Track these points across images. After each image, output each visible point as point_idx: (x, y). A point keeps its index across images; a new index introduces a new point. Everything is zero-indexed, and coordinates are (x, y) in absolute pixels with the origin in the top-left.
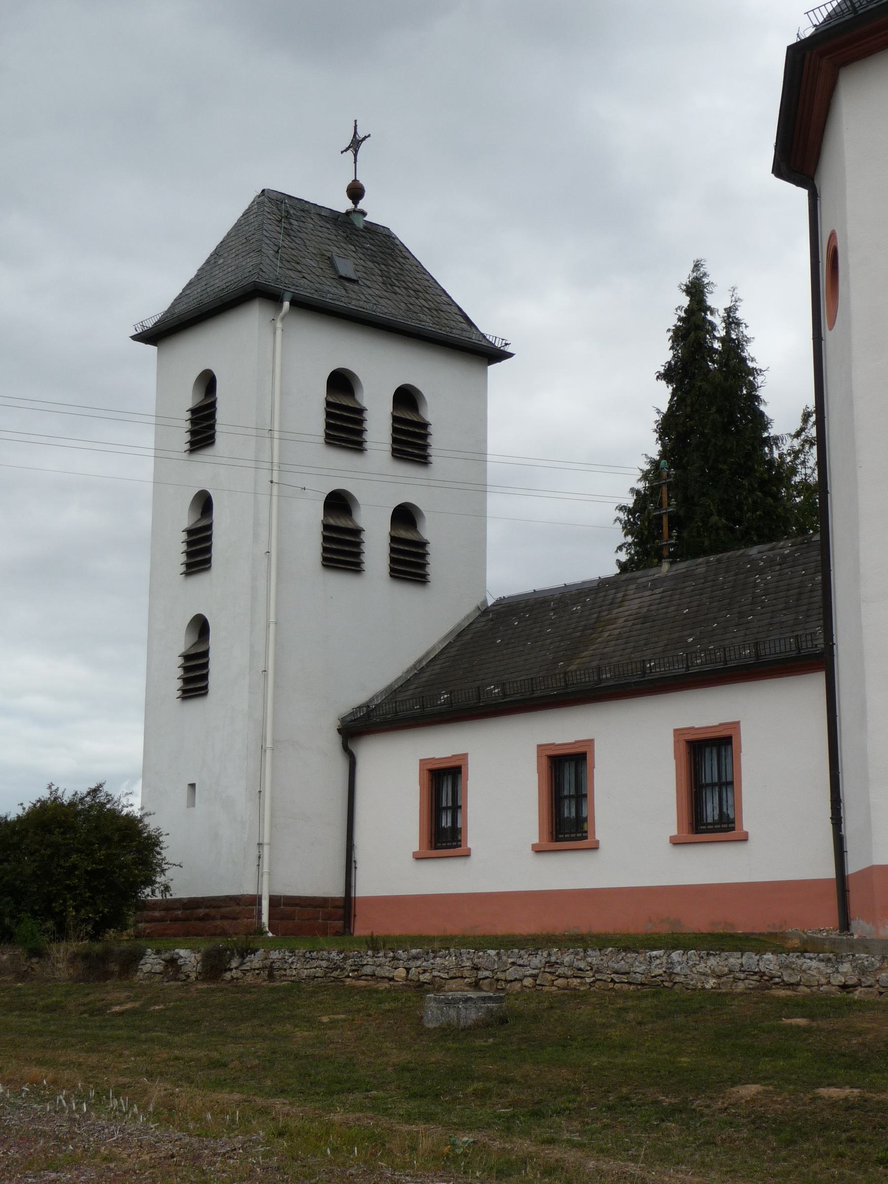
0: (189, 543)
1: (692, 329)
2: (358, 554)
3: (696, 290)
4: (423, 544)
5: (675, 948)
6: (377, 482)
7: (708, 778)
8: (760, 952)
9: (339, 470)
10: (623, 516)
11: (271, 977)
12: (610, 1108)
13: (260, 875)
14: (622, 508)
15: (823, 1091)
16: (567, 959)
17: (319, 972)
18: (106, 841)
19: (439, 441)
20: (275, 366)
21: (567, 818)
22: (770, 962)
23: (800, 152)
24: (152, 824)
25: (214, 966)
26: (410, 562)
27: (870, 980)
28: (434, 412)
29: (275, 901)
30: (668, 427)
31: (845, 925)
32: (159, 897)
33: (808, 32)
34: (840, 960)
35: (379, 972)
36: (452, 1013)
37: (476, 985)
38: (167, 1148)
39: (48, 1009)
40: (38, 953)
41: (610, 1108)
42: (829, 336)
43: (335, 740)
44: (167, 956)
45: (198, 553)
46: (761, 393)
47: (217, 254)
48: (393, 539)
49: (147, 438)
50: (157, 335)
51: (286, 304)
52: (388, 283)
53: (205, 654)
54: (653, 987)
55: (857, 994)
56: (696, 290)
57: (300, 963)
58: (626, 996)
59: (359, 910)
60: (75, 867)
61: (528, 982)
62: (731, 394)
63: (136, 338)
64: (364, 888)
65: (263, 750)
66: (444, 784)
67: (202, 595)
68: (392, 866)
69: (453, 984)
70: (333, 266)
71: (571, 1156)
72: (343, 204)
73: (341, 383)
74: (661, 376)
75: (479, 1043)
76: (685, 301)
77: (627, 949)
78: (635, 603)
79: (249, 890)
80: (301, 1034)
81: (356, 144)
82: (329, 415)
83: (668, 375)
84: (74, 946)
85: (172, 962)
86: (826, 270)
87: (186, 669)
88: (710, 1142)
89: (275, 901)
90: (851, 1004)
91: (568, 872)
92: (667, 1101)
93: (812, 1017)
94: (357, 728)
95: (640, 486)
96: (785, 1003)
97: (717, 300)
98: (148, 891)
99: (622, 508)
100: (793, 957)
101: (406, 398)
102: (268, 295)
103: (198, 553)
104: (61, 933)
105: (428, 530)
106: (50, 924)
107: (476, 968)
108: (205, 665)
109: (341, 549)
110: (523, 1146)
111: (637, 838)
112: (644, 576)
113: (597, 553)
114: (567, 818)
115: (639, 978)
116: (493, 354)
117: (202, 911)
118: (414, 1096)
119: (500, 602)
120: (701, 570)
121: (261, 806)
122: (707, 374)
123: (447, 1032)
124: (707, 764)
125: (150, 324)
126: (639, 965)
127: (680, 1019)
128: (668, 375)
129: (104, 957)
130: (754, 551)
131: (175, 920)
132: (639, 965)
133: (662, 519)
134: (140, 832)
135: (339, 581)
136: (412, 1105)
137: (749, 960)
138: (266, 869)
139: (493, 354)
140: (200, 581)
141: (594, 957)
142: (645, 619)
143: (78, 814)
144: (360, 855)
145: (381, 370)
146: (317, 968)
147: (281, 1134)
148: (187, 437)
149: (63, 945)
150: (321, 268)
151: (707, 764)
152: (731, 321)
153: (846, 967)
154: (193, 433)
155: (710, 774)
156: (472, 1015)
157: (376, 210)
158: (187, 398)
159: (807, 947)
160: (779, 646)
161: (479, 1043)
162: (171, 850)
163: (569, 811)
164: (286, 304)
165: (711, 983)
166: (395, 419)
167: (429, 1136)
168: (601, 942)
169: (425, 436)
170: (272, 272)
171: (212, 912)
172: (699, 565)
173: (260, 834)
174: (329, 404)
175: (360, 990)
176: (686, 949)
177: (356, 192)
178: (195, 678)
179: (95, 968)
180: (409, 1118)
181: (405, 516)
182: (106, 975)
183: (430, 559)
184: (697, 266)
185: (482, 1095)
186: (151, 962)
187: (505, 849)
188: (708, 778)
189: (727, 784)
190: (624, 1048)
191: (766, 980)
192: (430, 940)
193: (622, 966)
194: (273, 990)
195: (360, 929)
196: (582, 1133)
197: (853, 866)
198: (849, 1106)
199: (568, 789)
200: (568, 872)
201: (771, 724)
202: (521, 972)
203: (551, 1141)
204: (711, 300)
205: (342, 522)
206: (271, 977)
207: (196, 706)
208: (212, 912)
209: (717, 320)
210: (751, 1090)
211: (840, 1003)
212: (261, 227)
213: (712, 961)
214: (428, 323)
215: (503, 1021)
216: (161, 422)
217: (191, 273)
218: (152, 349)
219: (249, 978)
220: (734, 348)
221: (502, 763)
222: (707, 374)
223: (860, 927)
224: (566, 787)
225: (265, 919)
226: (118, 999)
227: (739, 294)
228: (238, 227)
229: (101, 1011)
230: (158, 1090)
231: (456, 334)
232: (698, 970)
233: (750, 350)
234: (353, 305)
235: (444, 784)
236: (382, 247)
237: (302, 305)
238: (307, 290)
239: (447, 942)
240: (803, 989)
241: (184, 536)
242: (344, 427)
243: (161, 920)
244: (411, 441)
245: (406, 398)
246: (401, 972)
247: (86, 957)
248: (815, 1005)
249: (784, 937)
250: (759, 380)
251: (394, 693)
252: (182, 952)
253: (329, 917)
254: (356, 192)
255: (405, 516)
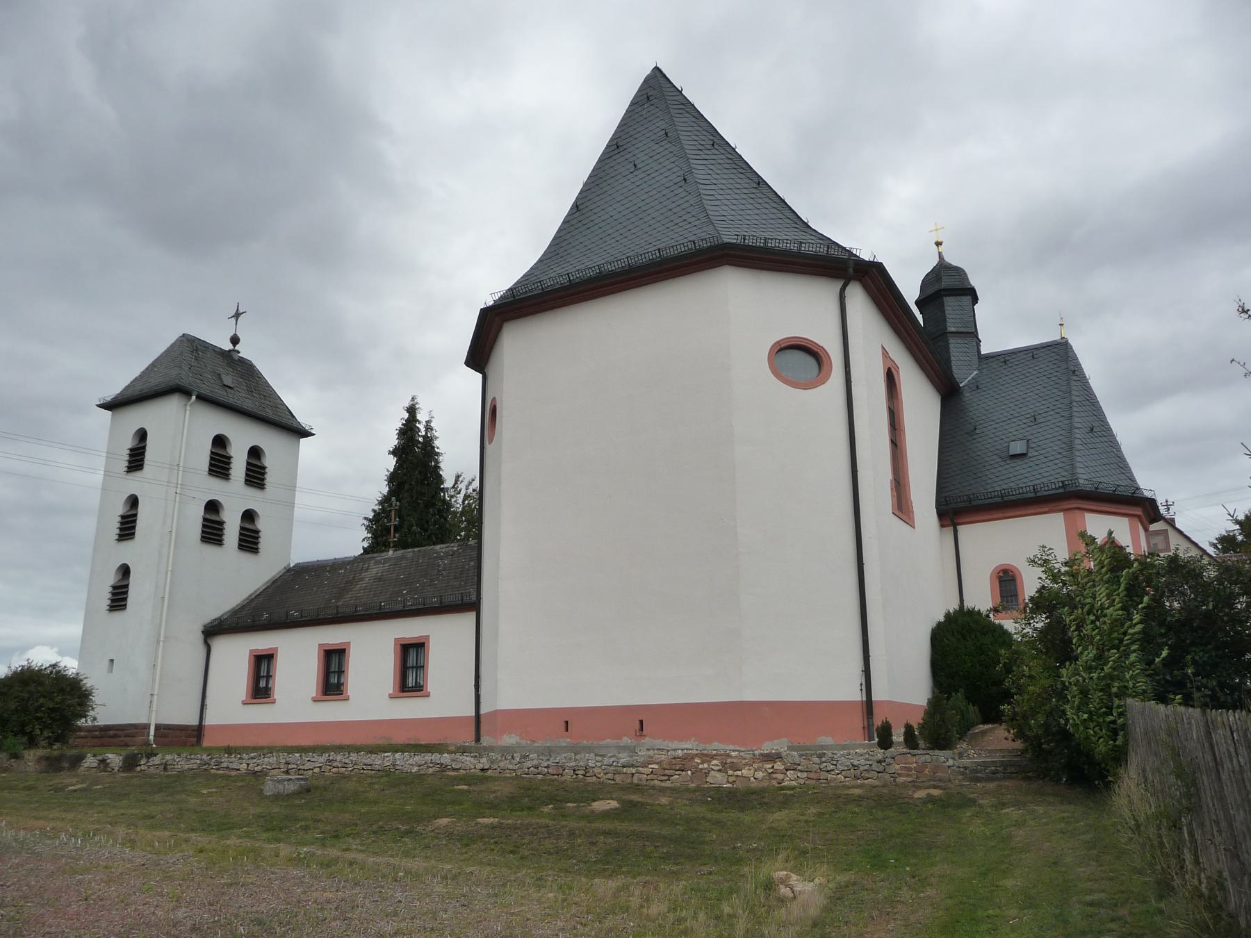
0: (122, 523)
1: (408, 430)
2: (221, 535)
3: (412, 410)
4: (257, 532)
5: (397, 751)
6: (235, 497)
7: (411, 664)
8: (441, 753)
9: (216, 489)
10: (366, 523)
11: (165, 769)
12: (374, 832)
13: (150, 712)
14: (366, 518)
15: (480, 820)
16: (339, 758)
17: (195, 766)
18: (62, 691)
19: (270, 478)
20: (182, 431)
21: (332, 681)
22: (446, 759)
23: (479, 357)
24: (88, 683)
25: (130, 763)
26: (249, 541)
27: (494, 767)
28: (269, 461)
29: (158, 727)
30: (393, 478)
31: (478, 739)
32: (90, 723)
33: (491, 303)
34: (481, 756)
35: (231, 766)
36: (281, 787)
37: (287, 772)
38: (139, 861)
39: (29, 788)
40: (16, 756)
41: (374, 832)
42: (488, 447)
43: (200, 637)
44: (100, 758)
45: (127, 528)
46: (441, 465)
47: (153, 365)
48: (242, 528)
49: (100, 463)
50: (112, 406)
51: (194, 397)
52: (250, 391)
53: (127, 586)
54: (385, 772)
55: (489, 773)
56: (412, 410)
57: (181, 761)
58: (371, 777)
59: (206, 732)
60: (42, 706)
61: (317, 770)
62: (425, 465)
63: (99, 406)
64: (209, 720)
65: (158, 641)
66: (263, 663)
67: (127, 553)
68: (229, 706)
69: (274, 772)
70: (220, 379)
71: (360, 856)
72: (228, 346)
73: (220, 442)
74: (390, 453)
75: (297, 802)
76: (406, 415)
77: (371, 752)
78: (374, 570)
79: (144, 721)
80: (193, 800)
81: (237, 315)
82: (212, 458)
83: (394, 452)
84: (40, 752)
85: (103, 761)
86: (490, 415)
87: (113, 594)
88: (427, 847)
89: (158, 727)
90: (487, 778)
91: (332, 712)
92: (403, 828)
93: (469, 785)
94: (213, 631)
95: (376, 508)
96: (455, 778)
97: (422, 417)
98: (83, 720)
99: (366, 518)
100: (458, 755)
101: (255, 453)
102: (185, 392)
103: (127, 528)
104: (32, 743)
105: (261, 524)
106: (25, 739)
107: (288, 763)
108: (126, 593)
109: (212, 532)
110: (333, 852)
111: (371, 693)
112: (379, 557)
113: (350, 541)
114: (332, 681)
115: (378, 767)
116: (306, 434)
117: (112, 733)
118: (267, 830)
119: (297, 565)
120: (410, 555)
121: (154, 674)
122: (415, 454)
123: (277, 797)
124: (411, 658)
125: (109, 399)
126: (378, 761)
127: (403, 788)
128: (394, 452)
129: (59, 759)
130: (438, 547)
131: (95, 737)
132: (378, 761)
133: (385, 528)
134: (80, 688)
135: (210, 549)
136: (265, 835)
137: (436, 757)
138: (154, 708)
139: (306, 434)
140: (127, 545)
141: (354, 757)
142: (380, 579)
143: (44, 676)
144: (208, 701)
145: (242, 437)
146: (194, 763)
147: (201, 851)
148: (126, 464)
149: (32, 752)
150: (213, 379)
151: (411, 658)
152: (428, 428)
153: (484, 760)
154: (130, 462)
155: (412, 660)
156: (292, 787)
157: (245, 351)
158: (128, 442)
159: (463, 750)
160: (452, 598)
161: (297, 802)
162: (96, 698)
163: (334, 680)
164: (194, 397)
165: (415, 769)
166: (248, 463)
167: (285, 850)
168: (357, 749)
169: (264, 474)
170: (187, 380)
171: (120, 733)
172: (409, 552)
173: (153, 689)
174: (212, 453)
175: (222, 776)
176: (403, 752)
177: (235, 340)
178: (119, 599)
179: (53, 765)
180: (269, 841)
181: (249, 516)
182: (60, 769)
183: (261, 540)
184: (413, 399)
185: (306, 829)
186: (90, 761)
187: (296, 698)
188: (411, 664)
189: (420, 667)
190: (376, 802)
191: (443, 768)
192: (262, 748)
193: (368, 761)
194: (168, 776)
195: (206, 743)
196: (362, 845)
197: (482, 712)
198: (494, 827)
199: (334, 667)
200: (332, 712)
201: (446, 637)
202: (313, 765)
203: (347, 850)
204: (419, 417)
205: (214, 517)
206: (165, 769)
207: (118, 615)
208: (120, 733)
209: (421, 427)
210: (446, 820)
211: (481, 778)
212: (181, 354)
213: (417, 758)
214: (269, 414)
215: (308, 790)
216: (110, 455)
217: (137, 373)
218: (109, 413)
219: (152, 770)
220: (429, 441)
221: (297, 654)
222: (415, 454)
223: (486, 740)
224: (333, 664)
225: (151, 738)
226: (71, 782)
227: (433, 414)
228: (167, 352)
229: (62, 789)
230: (121, 831)
231: (285, 421)
232: (408, 763)
233: (436, 443)
234: (231, 401)
235: (263, 663)
236: (247, 371)
237: (201, 398)
238: (205, 391)
239: (271, 750)
240: (462, 772)
241: (119, 519)
242: (219, 466)
243: (85, 737)
244: (256, 476)
245: (255, 453)
246: (244, 766)
247: (47, 759)
248: (468, 779)
249: (446, 745)
250: (441, 458)
251: (235, 612)
252: (110, 756)
253: (193, 735)
254: (235, 340)
255: (249, 516)
